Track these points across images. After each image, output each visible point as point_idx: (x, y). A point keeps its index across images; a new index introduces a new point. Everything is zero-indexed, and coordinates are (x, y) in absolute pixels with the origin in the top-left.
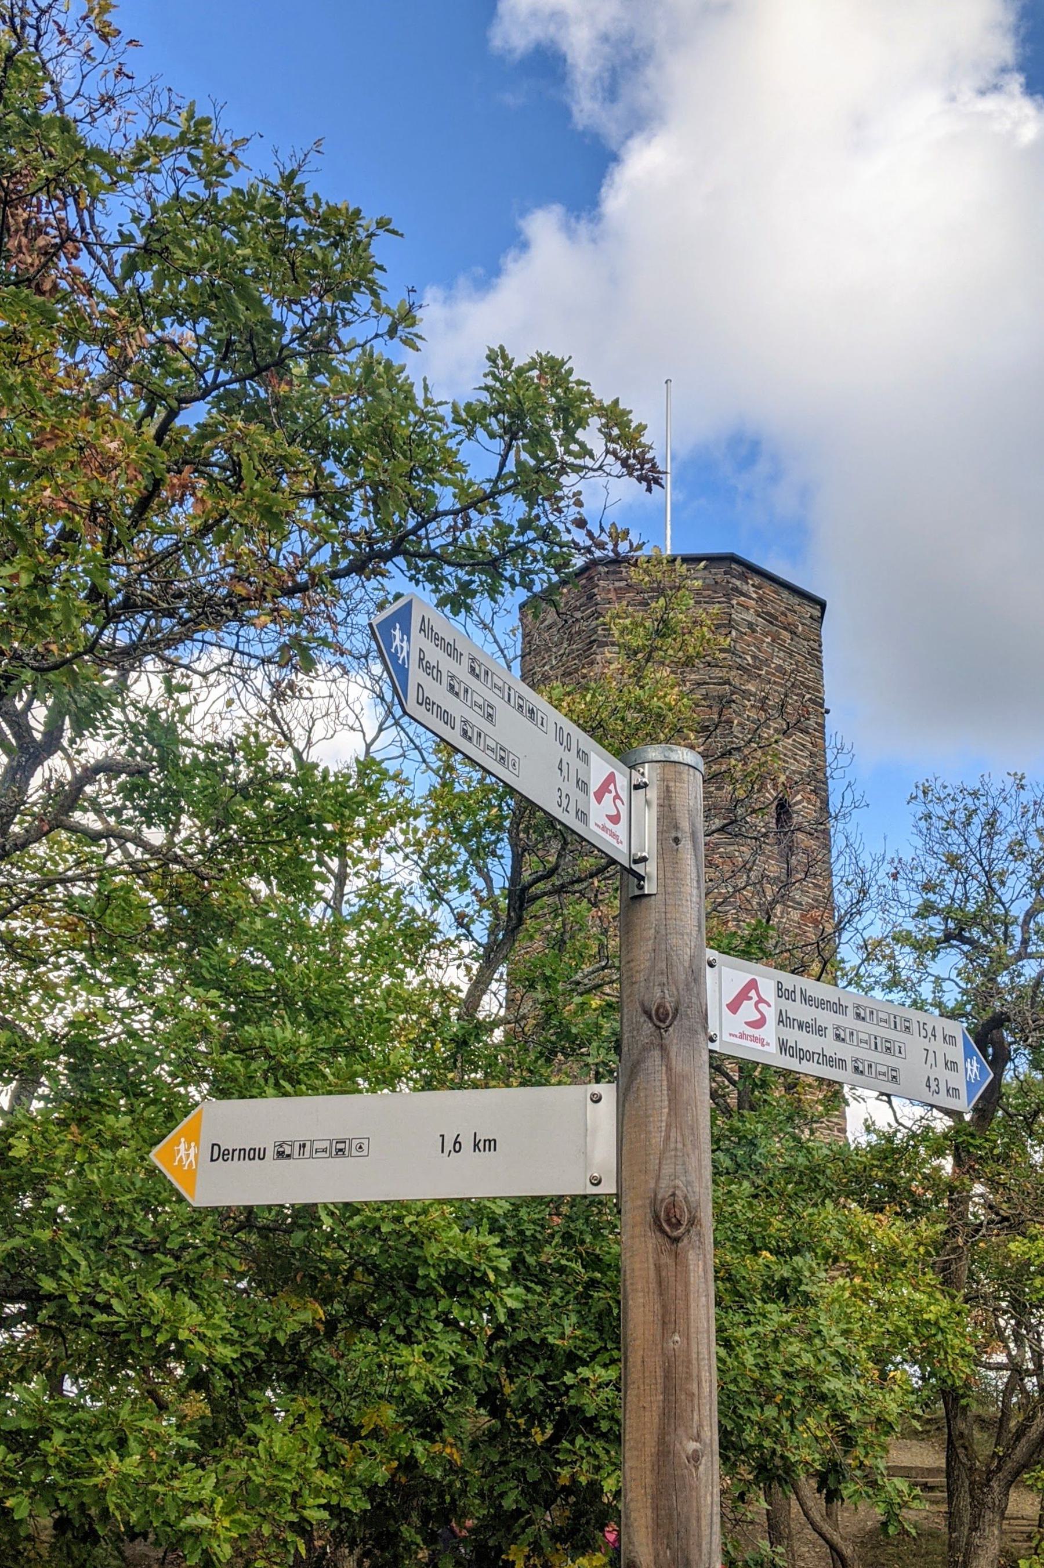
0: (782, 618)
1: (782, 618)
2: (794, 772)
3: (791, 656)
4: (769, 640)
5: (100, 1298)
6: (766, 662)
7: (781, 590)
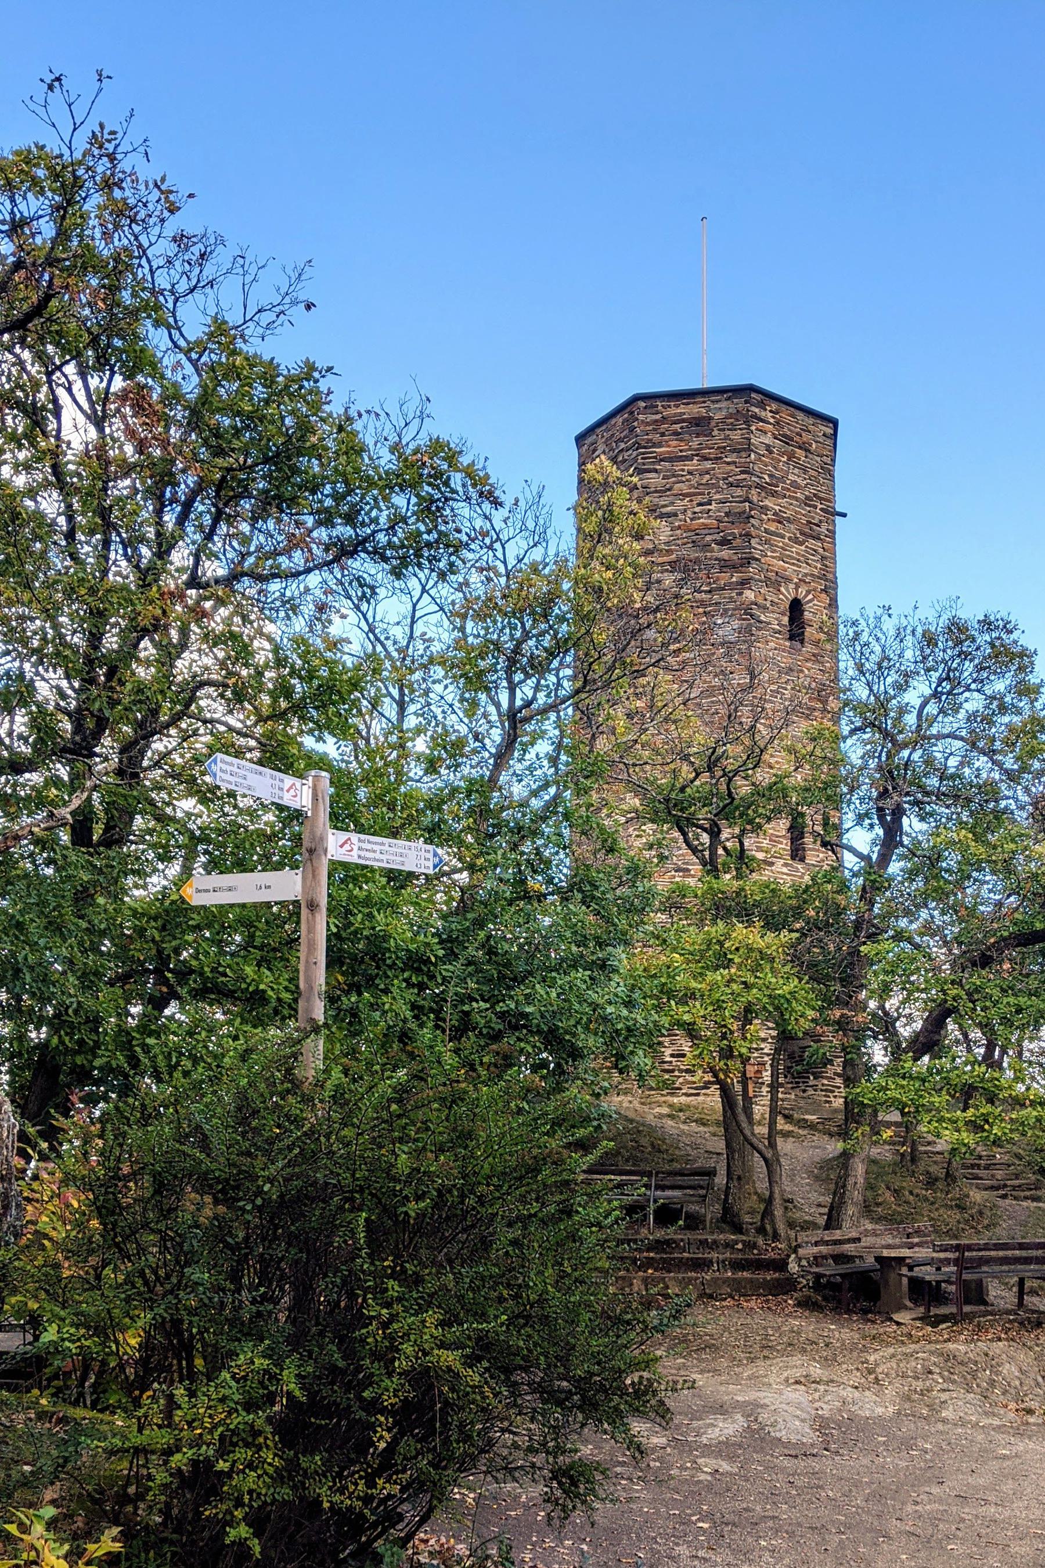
0: (797, 438)
1: (797, 438)
2: (806, 575)
3: (805, 472)
4: (785, 459)
5: (221, 969)
6: (782, 479)
7: (797, 413)
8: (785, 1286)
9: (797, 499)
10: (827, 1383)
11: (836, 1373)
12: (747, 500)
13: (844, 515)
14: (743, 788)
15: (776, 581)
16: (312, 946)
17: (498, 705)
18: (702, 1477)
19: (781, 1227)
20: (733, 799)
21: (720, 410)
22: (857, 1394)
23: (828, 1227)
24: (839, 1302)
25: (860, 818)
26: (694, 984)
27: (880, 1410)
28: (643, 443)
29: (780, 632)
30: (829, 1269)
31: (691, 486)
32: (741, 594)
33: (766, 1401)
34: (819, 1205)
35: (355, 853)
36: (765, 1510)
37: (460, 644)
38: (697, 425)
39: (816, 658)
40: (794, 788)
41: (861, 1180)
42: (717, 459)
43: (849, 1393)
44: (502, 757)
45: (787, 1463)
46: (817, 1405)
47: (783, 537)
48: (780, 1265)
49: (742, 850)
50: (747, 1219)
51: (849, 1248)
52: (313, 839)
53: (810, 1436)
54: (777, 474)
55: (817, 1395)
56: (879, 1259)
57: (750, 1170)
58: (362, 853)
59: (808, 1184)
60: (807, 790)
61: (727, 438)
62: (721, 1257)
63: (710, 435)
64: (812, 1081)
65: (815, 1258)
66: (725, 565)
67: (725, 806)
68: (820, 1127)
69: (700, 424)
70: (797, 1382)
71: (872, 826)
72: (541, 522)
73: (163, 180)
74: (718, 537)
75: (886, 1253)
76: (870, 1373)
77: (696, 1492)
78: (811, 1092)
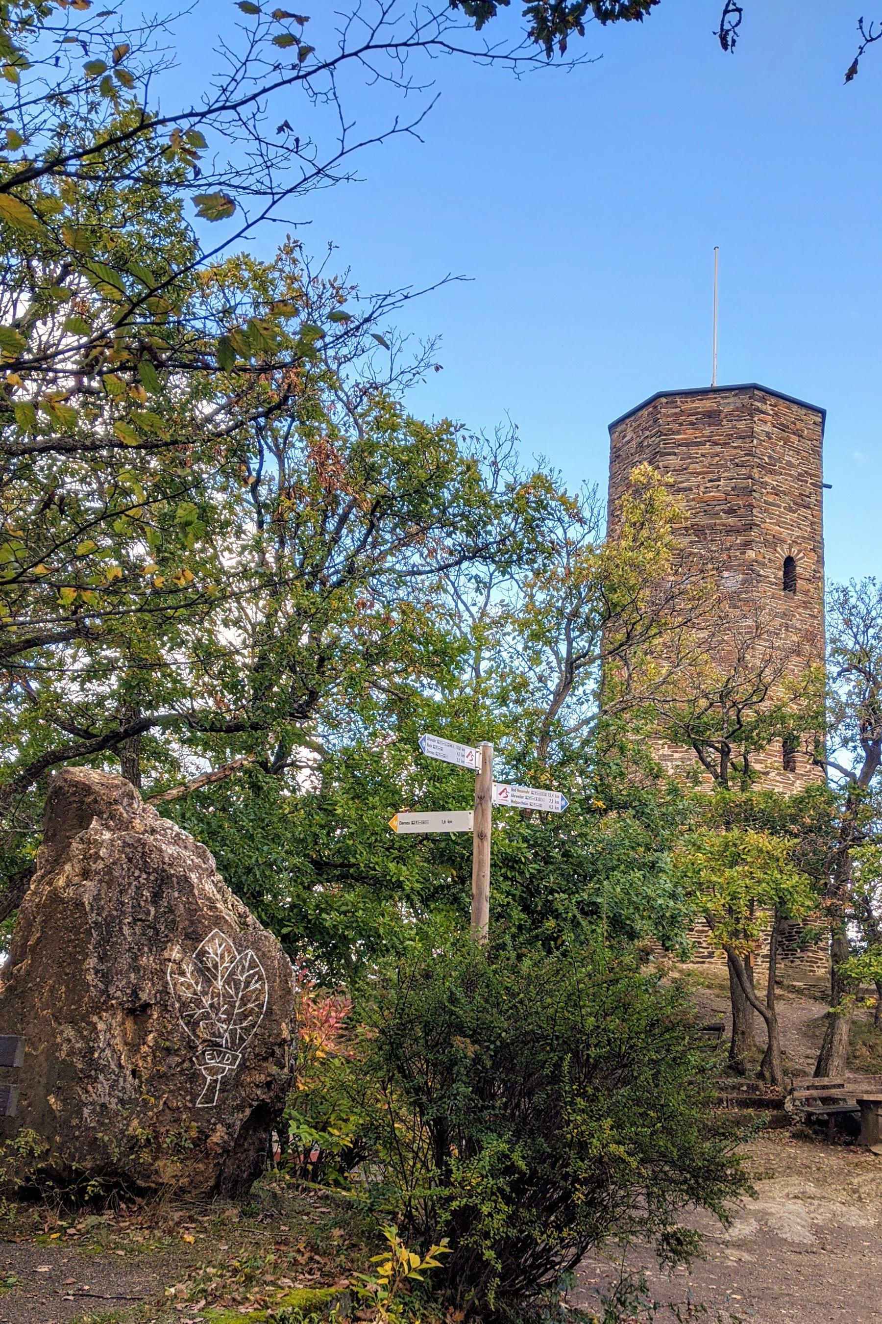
0: (792, 426)
1: (792, 426)
2: (798, 537)
3: (798, 453)
6: (779, 460)
7: (792, 405)
8: (782, 1122)
9: (791, 476)
10: (820, 1199)
11: (828, 1191)
12: (750, 477)
13: (830, 487)
14: (749, 716)
15: (773, 542)
16: (481, 863)
17: (556, 653)
18: (730, 1263)
19: (779, 1075)
20: (741, 726)
21: (729, 404)
22: (844, 1209)
23: (817, 1074)
24: (826, 1135)
25: (845, 742)
26: (714, 878)
27: (863, 1222)
28: (665, 432)
29: (776, 584)
30: (818, 1109)
31: (704, 466)
32: (743, 553)
33: (773, 1210)
34: (807, 1057)
35: (509, 799)
36: (781, 1289)
37: (529, 607)
38: (710, 417)
39: (806, 605)
40: (791, 716)
41: (845, 1037)
42: (726, 444)
43: (838, 1208)
44: (559, 695)
45: (794, 1257)
46: (812, 1215)
47: (779, 507)
48: (778, 1104)
49: (747, 765)
50: (749, 1066)
51: (835, 1093)
52: (483, 791)
53: (809, 1239)
54: (775, 455)
55: (812, 1208)
56: (860, 1102)
57: (750, 1026)
58: (514, 799)
59: (797, 1039)
60: (801, 718)
61: (734, 427)
62: (730, 1096)
63: (720, 424)
64: (799, 953)
65: (807, 1099)
66: (731, 531)
67: (734, 732)
68: (806, 992)
69: (712, 417)
70: (796, 1197)
71: (855, 748)
72: (596, 511)
73: (335, 279)
74: (725, 507)
75: (866, 1097)
76: (854, 1193)
77: (728, 1274)
78: (798, 962)
